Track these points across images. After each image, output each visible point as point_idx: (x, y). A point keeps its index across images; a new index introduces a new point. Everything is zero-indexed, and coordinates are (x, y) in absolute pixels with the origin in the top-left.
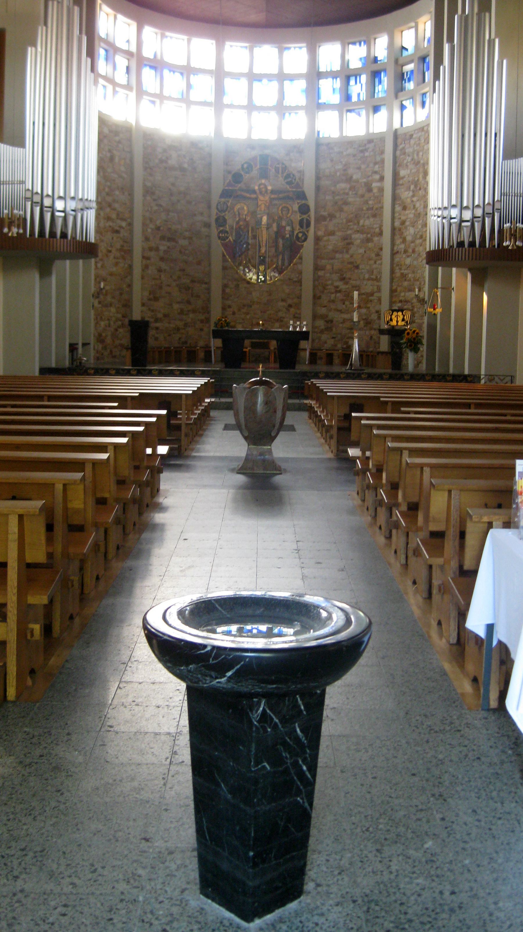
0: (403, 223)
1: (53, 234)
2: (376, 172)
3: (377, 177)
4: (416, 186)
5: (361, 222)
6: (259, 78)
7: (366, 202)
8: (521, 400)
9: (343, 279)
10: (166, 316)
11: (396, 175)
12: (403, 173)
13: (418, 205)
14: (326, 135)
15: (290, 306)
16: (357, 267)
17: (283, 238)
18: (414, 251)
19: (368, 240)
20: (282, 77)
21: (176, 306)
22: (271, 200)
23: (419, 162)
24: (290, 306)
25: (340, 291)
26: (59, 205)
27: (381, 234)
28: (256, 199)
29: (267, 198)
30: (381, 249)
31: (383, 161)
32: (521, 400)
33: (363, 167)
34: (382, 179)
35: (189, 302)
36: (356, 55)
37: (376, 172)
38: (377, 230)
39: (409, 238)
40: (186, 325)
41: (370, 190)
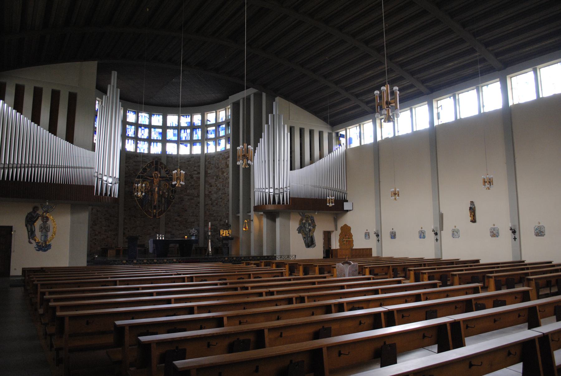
0: (210, 192)
1: (106, 194)
2: (195, 170)
3: (196, 172)
4: (217, 177)
5: (188, 191)
6: (141, 126)
7: (190, 183)
8: (557, 271)
9: (179, 216)
10: (99, 233)
11: (206, 173)
12: (209, 171)
13: (218, 185)
14: (170, 153)
15: (154, 228)
16: (186, 210)
17: (165, 198)
18: (217, 204)
19: (192, 199)
20: (150, 127)
21: (104, 228)
22: (160, 181)
23: (218, 168)
24: (154, 228)
25: (178, 221)
26: (105, 178)
27: (198, 196)
28: (153, 180)
29: (158, 180)
30: (199, 203)
31: (199, 166)
32: (557, 271)
33: (189, 168)
34: (199, 173)
35: (109, 226)
36: (185, 121)
37: (195, 170)
38: (196, 195)
39: (214, 199)
40: (107, 237)
41: (192, 178)
